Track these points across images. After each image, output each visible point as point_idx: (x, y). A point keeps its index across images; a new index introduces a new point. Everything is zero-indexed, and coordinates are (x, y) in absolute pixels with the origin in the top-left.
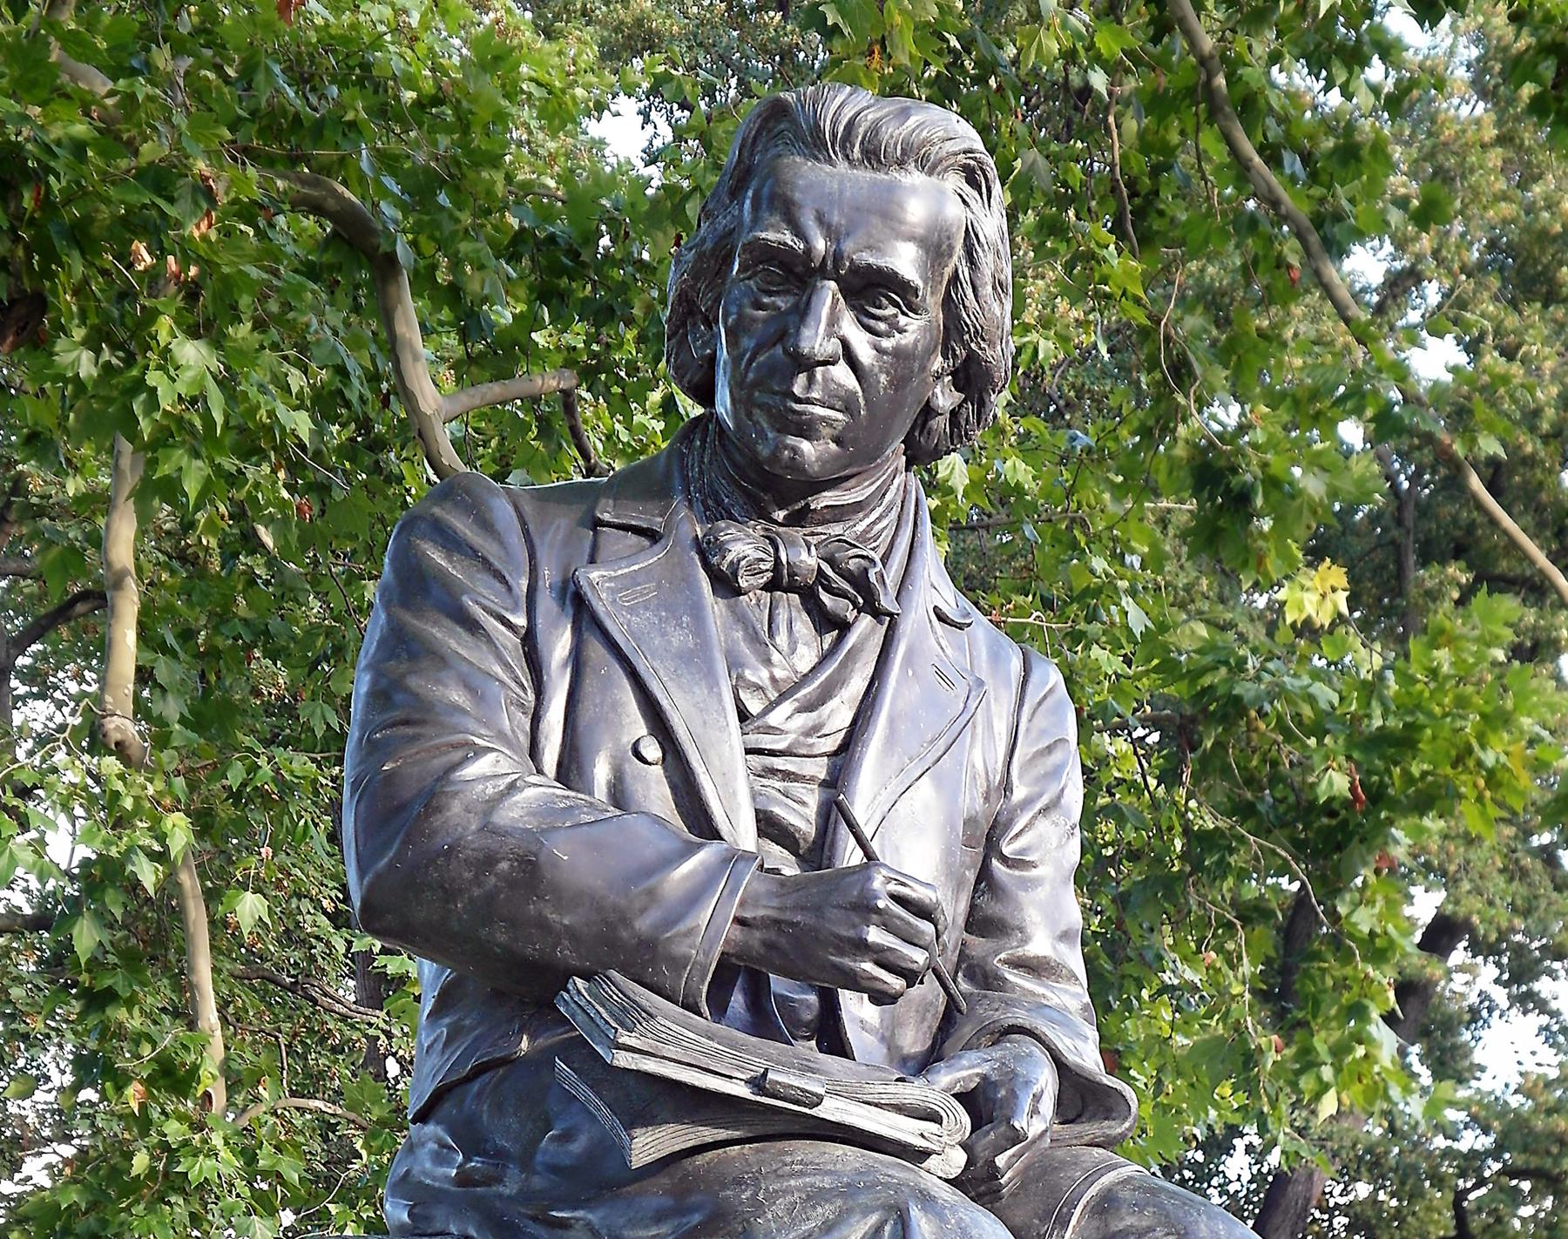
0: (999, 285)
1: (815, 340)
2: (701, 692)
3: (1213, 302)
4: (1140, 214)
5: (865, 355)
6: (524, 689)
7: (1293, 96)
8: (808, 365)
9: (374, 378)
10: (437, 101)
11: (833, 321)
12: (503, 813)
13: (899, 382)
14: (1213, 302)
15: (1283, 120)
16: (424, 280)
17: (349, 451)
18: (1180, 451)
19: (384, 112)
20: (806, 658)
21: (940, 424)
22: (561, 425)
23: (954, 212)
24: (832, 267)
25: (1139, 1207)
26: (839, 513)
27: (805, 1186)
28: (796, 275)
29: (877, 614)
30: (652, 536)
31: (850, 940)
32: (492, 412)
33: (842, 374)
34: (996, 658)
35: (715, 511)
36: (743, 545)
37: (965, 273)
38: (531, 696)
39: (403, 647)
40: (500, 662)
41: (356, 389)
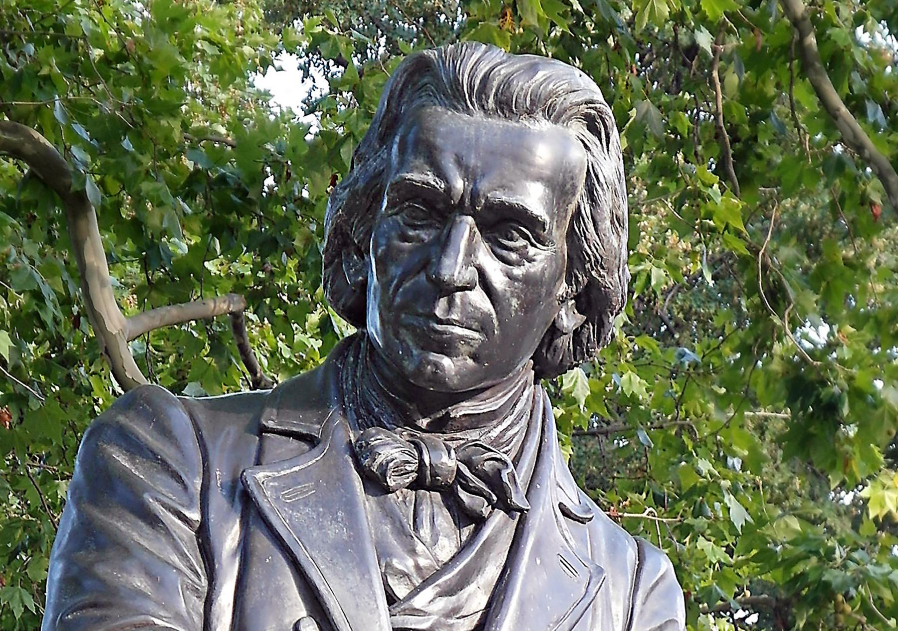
0: (616, 220)
1: (455, 268)
2: (354, 578)
3: (806, 236)
4: (740, 157)
5: (499, 281)
7: (875, 53)
8: (448, 290)
9: (66, 302)
10: (122, 57)
11: (471, 251)
13: (528, 306)
14: (806, 236)
15: (867, 74)
16: (110, 216)
17: (44, 366)
18: (776, 366)
19: (76, 67)
20: (446, 549)
21: (565, 342)
22: (230, 343)
23: (577, 154)
24: (470, 203)
26: (476, 421)
28: (439, 210)
29: (509, 509)
30: (311, 441)
32: (170, 331)
33: (478, 297)
34: (614, 549)
35: (366, 419)
36: (391, 449)
37: (586, 209)
38: (204, 582)
39: (92, 538)
40: (178, 553)
41: (51, 311)
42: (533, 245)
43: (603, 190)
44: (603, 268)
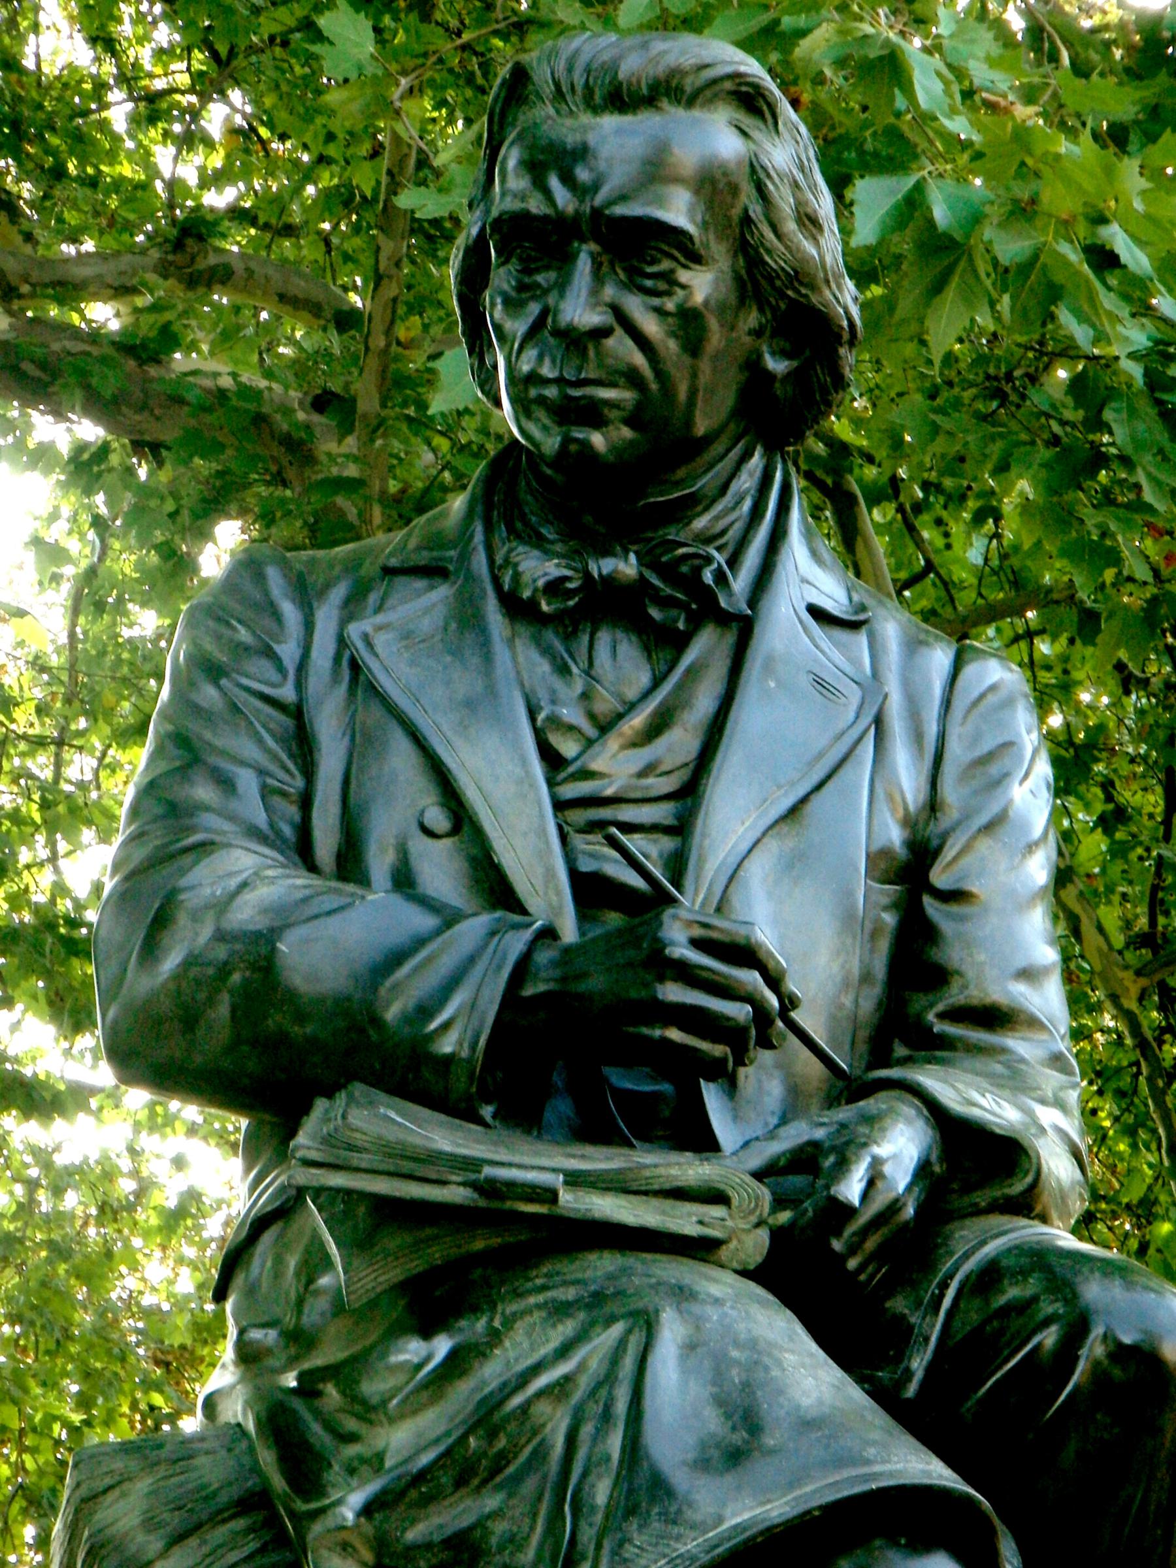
5: (651, 326)
6: (288, 771)
12: (230, 916)
25: (1023, 1273)
27: (546, 1303)
31: (640, 1003)
33: (621, 346)
37: (756, 211)
38: (299, 782)
42: (685, 267)
43: (774, 183)
44: (801, 284)
